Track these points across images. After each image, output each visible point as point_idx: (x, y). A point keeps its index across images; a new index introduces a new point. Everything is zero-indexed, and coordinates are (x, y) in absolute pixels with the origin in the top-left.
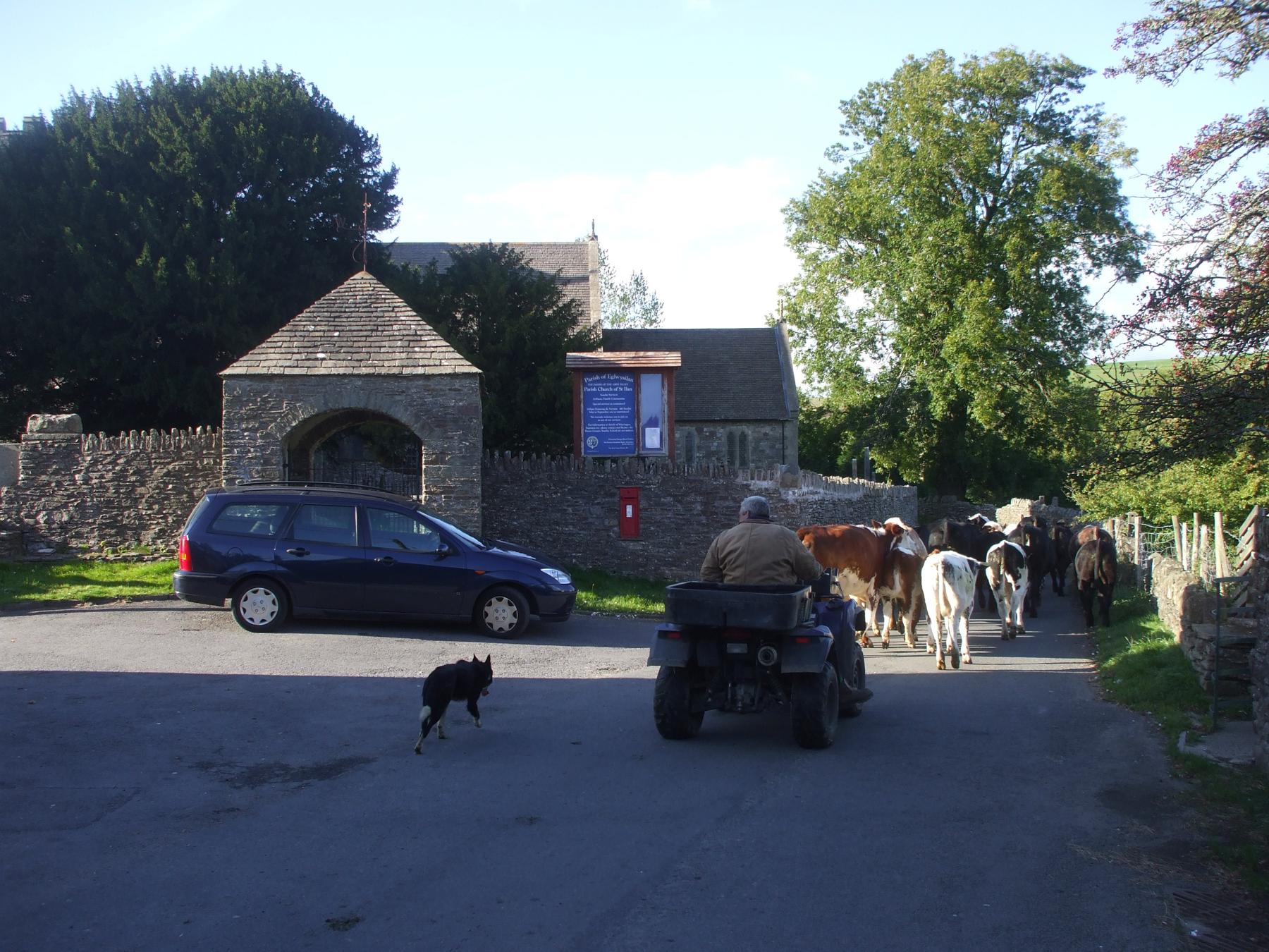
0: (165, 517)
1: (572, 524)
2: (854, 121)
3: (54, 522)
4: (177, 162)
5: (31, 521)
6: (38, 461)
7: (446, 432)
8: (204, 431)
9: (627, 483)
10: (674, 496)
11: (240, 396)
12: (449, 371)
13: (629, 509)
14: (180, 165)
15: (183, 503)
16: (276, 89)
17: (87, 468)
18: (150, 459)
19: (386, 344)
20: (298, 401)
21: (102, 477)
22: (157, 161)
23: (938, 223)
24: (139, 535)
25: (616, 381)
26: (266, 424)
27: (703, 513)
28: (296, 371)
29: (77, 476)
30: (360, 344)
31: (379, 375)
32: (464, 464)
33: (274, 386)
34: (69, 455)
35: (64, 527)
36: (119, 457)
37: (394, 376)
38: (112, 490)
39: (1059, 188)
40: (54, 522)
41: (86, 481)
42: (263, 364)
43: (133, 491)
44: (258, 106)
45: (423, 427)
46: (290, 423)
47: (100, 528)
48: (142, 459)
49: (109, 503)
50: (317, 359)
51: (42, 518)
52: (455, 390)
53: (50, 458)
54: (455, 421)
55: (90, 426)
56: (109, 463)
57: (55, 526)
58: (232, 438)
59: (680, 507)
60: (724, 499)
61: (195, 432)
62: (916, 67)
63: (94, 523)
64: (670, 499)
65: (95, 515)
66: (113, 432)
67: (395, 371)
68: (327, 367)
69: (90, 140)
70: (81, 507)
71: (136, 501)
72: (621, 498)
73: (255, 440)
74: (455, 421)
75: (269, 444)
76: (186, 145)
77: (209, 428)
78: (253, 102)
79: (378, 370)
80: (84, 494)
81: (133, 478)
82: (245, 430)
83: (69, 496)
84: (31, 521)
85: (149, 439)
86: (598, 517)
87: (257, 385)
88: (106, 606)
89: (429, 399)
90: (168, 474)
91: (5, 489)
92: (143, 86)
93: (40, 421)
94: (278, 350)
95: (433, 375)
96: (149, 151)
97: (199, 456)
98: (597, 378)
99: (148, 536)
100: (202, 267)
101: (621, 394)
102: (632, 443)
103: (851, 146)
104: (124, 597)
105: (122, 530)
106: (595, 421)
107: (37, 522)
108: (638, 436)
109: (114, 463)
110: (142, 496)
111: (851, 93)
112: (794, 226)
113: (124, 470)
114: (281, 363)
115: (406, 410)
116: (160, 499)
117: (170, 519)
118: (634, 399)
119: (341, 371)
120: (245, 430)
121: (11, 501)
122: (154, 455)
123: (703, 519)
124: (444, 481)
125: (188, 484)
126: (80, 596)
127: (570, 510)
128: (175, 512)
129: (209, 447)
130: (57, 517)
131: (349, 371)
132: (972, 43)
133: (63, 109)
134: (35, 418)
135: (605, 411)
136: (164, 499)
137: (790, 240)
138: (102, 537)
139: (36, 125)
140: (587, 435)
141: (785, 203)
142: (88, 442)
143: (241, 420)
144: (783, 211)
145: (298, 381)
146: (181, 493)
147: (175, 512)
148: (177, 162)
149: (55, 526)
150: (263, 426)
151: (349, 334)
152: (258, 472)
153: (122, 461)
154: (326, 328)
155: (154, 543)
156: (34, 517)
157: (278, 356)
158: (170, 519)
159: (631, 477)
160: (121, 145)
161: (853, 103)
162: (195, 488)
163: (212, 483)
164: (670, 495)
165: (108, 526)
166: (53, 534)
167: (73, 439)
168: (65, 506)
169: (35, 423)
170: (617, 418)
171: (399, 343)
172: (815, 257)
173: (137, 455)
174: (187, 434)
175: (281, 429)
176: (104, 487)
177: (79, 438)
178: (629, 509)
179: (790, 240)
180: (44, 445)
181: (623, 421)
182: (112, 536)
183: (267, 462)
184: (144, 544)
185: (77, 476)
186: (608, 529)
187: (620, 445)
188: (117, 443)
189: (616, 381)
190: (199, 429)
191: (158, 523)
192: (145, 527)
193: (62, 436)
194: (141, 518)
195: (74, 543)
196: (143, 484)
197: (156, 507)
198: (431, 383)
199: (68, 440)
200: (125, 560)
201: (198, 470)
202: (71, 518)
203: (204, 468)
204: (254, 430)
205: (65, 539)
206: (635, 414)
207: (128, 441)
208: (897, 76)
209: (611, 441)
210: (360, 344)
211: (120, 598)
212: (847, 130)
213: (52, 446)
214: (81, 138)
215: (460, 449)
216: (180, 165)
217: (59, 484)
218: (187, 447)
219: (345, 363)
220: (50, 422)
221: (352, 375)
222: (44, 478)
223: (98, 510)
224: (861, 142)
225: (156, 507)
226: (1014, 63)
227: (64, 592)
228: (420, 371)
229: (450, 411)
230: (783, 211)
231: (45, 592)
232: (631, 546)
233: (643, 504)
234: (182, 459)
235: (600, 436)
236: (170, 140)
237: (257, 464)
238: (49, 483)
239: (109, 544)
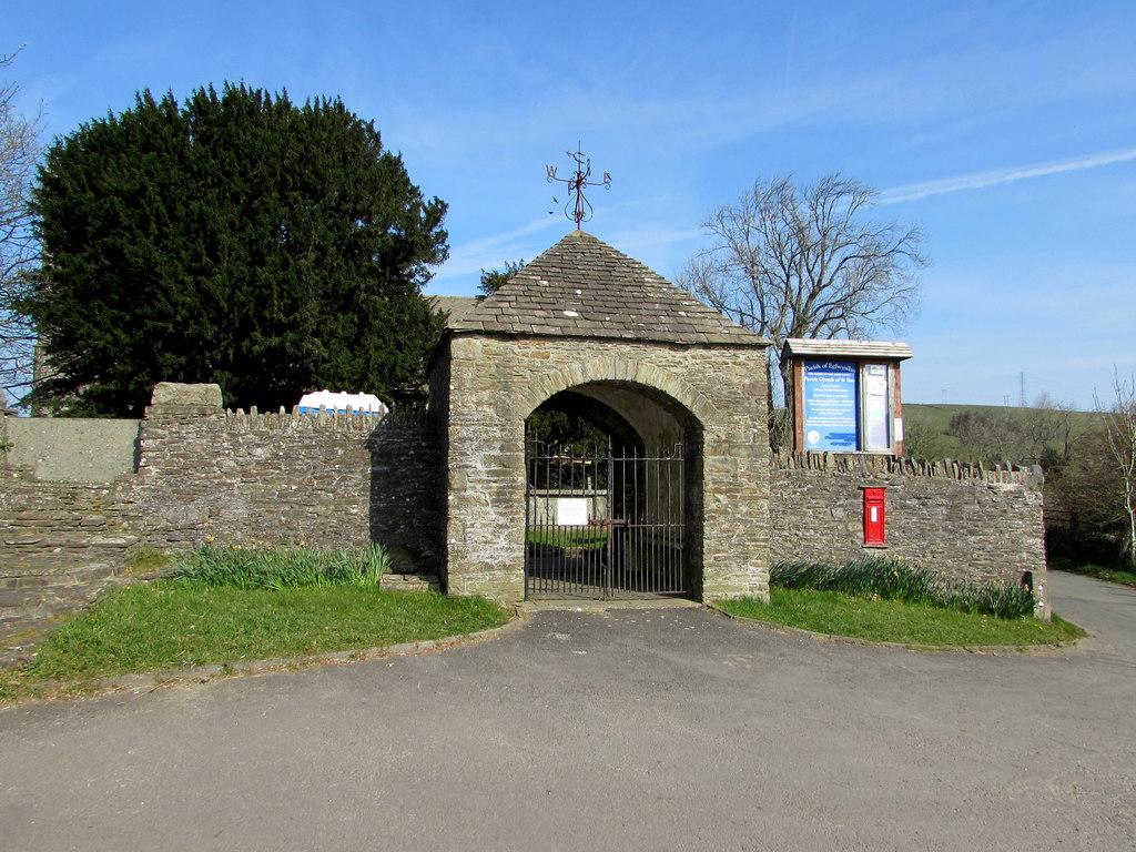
9: (870, 482)
98: (818, 366)
186: (850, 535)
233: (888, 506)
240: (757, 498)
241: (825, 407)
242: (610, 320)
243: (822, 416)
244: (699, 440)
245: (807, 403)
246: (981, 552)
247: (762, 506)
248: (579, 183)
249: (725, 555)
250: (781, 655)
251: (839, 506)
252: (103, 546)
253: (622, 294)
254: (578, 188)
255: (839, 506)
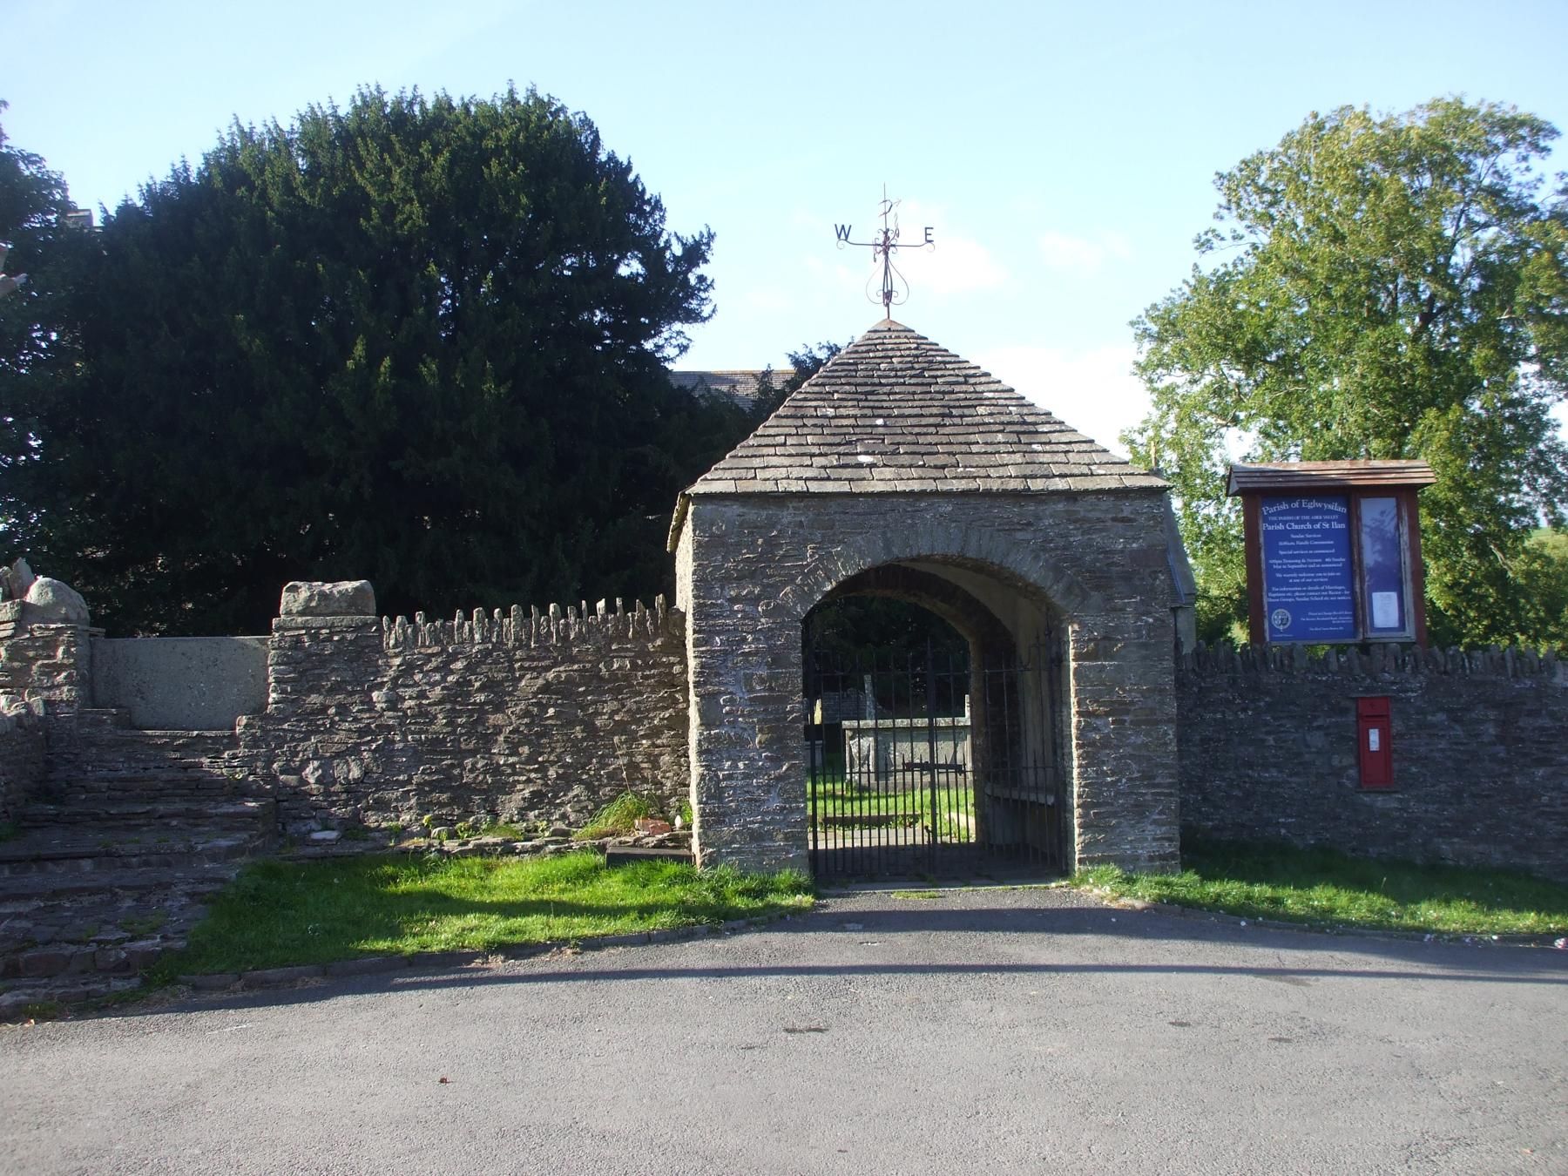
0: (542, 769)
1: (1275, 765)
2: (1233, 202)
3: (334, 782)
4: (399, 218)
5: (292, 779)
6: (305, 667)
7: (1110, 599)
8: (610, 608)
9: (1367, 690)
10: (1449, 711)
11: (725, 535)
12: (1113, 484)
13: (1374, 737)
14: (405, 222)
15: (575, 743)
16: (534, 118)
17: (394, 680)
18: (511, 661)
19: (977, 438)
20: (834, 543)
21: (422, 695)
22: (369, 218)
23: (1371, 336)
24: (494, 803)
25: (1317, 511)
26: (777, 588)
27: (1501, 739)
28: (830, 487)
29: (375, 695)
30: (929, 439)
31: (988, 493)
32: (1145, 658)
33: (787, 516)
34: (361, 657)
35: (353, 790)
36: (453, 657)
37: (1015, 494)
38: (441, 720)
39: (1550, 278)
40: (334, 782)
41: (393, 703)
42: (760, 474)
43: (481, 720)
44: (514, 138)
45: (1069, 590)
46: (820, 585)
47: (420, 790)
48: (496, 662)
49: (436, 744)
50: (860, 466)
51: (311, 773)
52: (1123, 520)
53: (324, 661)
54: (1127, 578)
55: (392, 602)
56: (436, 670)
57: (337, 787)
58: (708, 616)
59: (1458, 730)
60: (1534, 713)
61: (592, 610)
62: (1319, 127)
63: (409, 782)
64: (1441, 717)
65: (409, 769)
66: (440, 610)
67: (1013, 485)
68: (881, 480)
69: (264, 191)
70: (385, 753)
71: (487, 740)
72: (1359, 716)
73: (755, 619)
74: (1127, 578)
75: (783, 626)
76: (413, 194)
77: (619, 602)
78: (505, 135)
79: (980, 484)
80: (390, 728)
81: (481, 698)
82: (733, 600)
83: (362, 733)
84: (292, 779)
85: (511, 624)
86: (1319, 752)
87: (753, 514)
88: (540, 964)
89: (1077, 538)
90: (546, 688)
91: (244, 720)
92: (342, 113)
93: (304, 593)
94: (779, 450)
95: (1086, 492)
96: (355, 203)
97: (604, 655)
98: (1284, 506)
99: (510, 805)
100: (445, 375)
101: (1326, 534)
102: (1349, 620)
103: (1228, 236)
104: (564, 942)
105: (462, 796)
106: (1285, 582)
107: (304, 782)
108: (1359, 610)
109: (445, 669)
110: (498, 730)
111: (1230, 165)
112: (1148, 345)
113: (464, 683)
114: (795, 472)
115: (1037, 558)
116: (535, 735)
117: (552, 773)
118: (1349, 543)
119: (916, 486)
120: (733, 600)
121: (255, 743)
122: (519, 654)
123: (1501, 751)
124: (1111, 691)
125: (584, 708)
126: (476, 939)
127: (1271, 740)
128: (560, 758)
129: (621, 637)
130: (339, 771)
131: (929, 486)
132: (1400, 95)
133: (220, 150)
134: (295, 589)
135: (1300, 564)
136: (540, 735)
137: (1138, 364)
138: (424, 808)
139: (126, 210)
140: (1273, 607)
141: (1138, 309)
142: (394, 631)
143: (726, 580)
144: (1132, 324)
145: (833, 506)
146: (570, 723)
147: (560, 758)
148: (399, 218)
149: (337, 787)
150: (770, 591)
151: (900, 422)
152: (762, 681)
153: (459, 665)
154: (857, 412)
155: (523, 818)
156: (298, 771)
157: (787, 461)
158: (552, 773)
159: (1374, 679)
160: (313, 196)
161: (1230, 177)
162: (597, 713)
163: (630, 704)
164: (1442, 709)
165: (435, 786)
166: (333, 804)
167: (367, 625)
168: (355, 750)
169: (295, 598)
170: (1322, 577)
171: (1000, 437)
172: (1171, 389)
173: (487, 653)
174: (579, 615)
175: (801, 596)
176: (426, 714)
177: (380, 623)
178: (1374, 737)
179: (1138, 364)
180: (314, 637)
181: (1332, 581)
182: (441, 805)
183: (777, 660)
184: (502, 819)
185: (375, 695)
186: (1338, 772)
187: (1329, 624)
188: (450, 632)
189: (1317, 511)
190: (601, 604)
191: (529, 781)
192: (508, 789)
193: (347, 620)
194: (496, 770)
195: (372, 820)
196: (499, 707)
197: (525, 750)
198: (1080, 508)
199: (357, 629)
200: (481, 850)
201: (601, 679)
202: (366, 773)
203: (614, 676)
204: (754, 600)
205: (356, 813)
206: (1353, 567)
207: (470, 629)
208: (1287, 143)
209: (1313, 616)
210: (929, 439)
211: (560, 943)
212: (1224, 212)
213: (329, 639)
214: (251, 188)
215: (1138, 630)
216: (405, 222)
217: (343, 710)
218: (581, 638)
219: (914, 472)
220: (323, 595)
221: (936, 494)
222: (315, 699)
223: (417, 755)
224: (1241, 230)
225: (525, 750)
226: (1456, 116)
227: (445, 933)
228: (1060, 484)
229: (1117, 558)
230: (1132, 324)
231: (396, 933)
232: (1380, 801)
233: (1397, 726)
234: (573, 660)
235: (1296, 608)
236: (386, 187)
237: (759, 664)
238: (324, 709)
239: (438, 821)
240: (1157, 722)
241: (1298, 571)
242: (885, 426)
243: (1294, 585)
244: (218, 183)
245: (1269, 566)
246: (1554, 794)
247: (1166, 733)
248: (886, 247)
249: (1110, 808)
250: (1338, 238)
251: (1319, 728)
252: (228, 815)
253: (948, 421)
254: (886, 254)
255: (1319, 728)
